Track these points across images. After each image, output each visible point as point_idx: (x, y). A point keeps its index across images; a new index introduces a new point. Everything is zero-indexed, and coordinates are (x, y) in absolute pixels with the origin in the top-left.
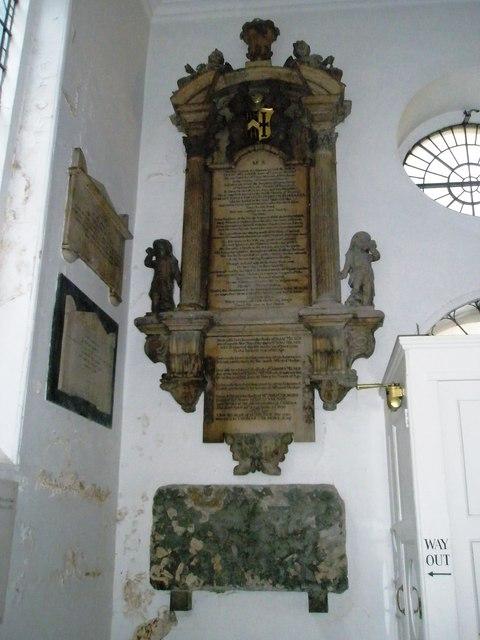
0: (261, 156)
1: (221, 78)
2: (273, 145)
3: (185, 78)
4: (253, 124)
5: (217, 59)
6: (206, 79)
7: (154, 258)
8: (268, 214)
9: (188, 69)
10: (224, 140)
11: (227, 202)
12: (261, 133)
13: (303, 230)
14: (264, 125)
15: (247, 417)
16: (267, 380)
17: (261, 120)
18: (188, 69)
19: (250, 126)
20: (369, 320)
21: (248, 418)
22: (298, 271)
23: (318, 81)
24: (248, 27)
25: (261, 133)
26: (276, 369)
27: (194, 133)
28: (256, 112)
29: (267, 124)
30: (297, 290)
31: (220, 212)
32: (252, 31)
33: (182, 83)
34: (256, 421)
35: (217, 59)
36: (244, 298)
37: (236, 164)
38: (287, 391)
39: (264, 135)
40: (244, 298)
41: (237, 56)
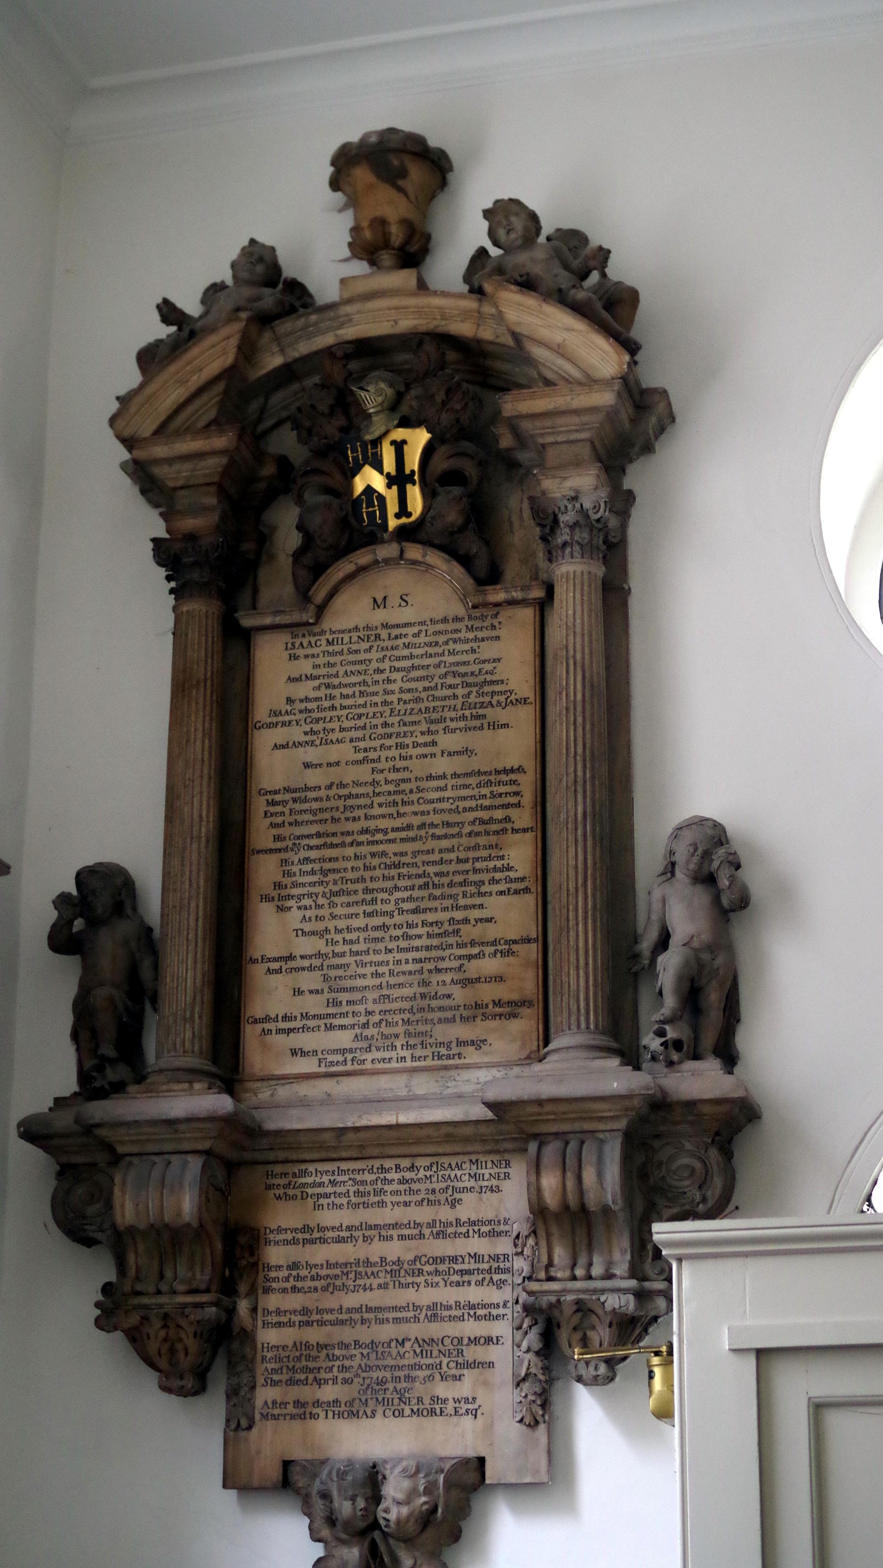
0: (395, 581)
1: (267, 335)
2: (429, 543)
3: (158, 343)
4: (371, 479)
5: (261, 267)
6: (213, 356)
7: (78, 924)
8: (418, 768)
9: (168, 312)
10: (286, 527)
11: (296, 734)
12: (392, 507)
13: (524, 817)
14: (399, 480)
15: (351, 1411)
16: (409, 1296)
17: (389, 464)
18: (168, 312)
19: (359, 485)
20: (706, 1109)
21: (354, 1415)
22: (506, 948)
23: (558, 337)
24: (346, 161)
25: (392, 507)
26: (435, 1260)
27: (190, 523)
28: (377, 442)
29: (410, 478)
30: (509, 1009)
31: (275, 763)
32: (362, 175)
33: (150, 358)
34: (379, 1419)
35: (261, 267)
36: (344, 1039)
37: (321, 610)
38: (471, 1328)
39: (404, 511)
40: (344, 1039)
41: (319, 245)
